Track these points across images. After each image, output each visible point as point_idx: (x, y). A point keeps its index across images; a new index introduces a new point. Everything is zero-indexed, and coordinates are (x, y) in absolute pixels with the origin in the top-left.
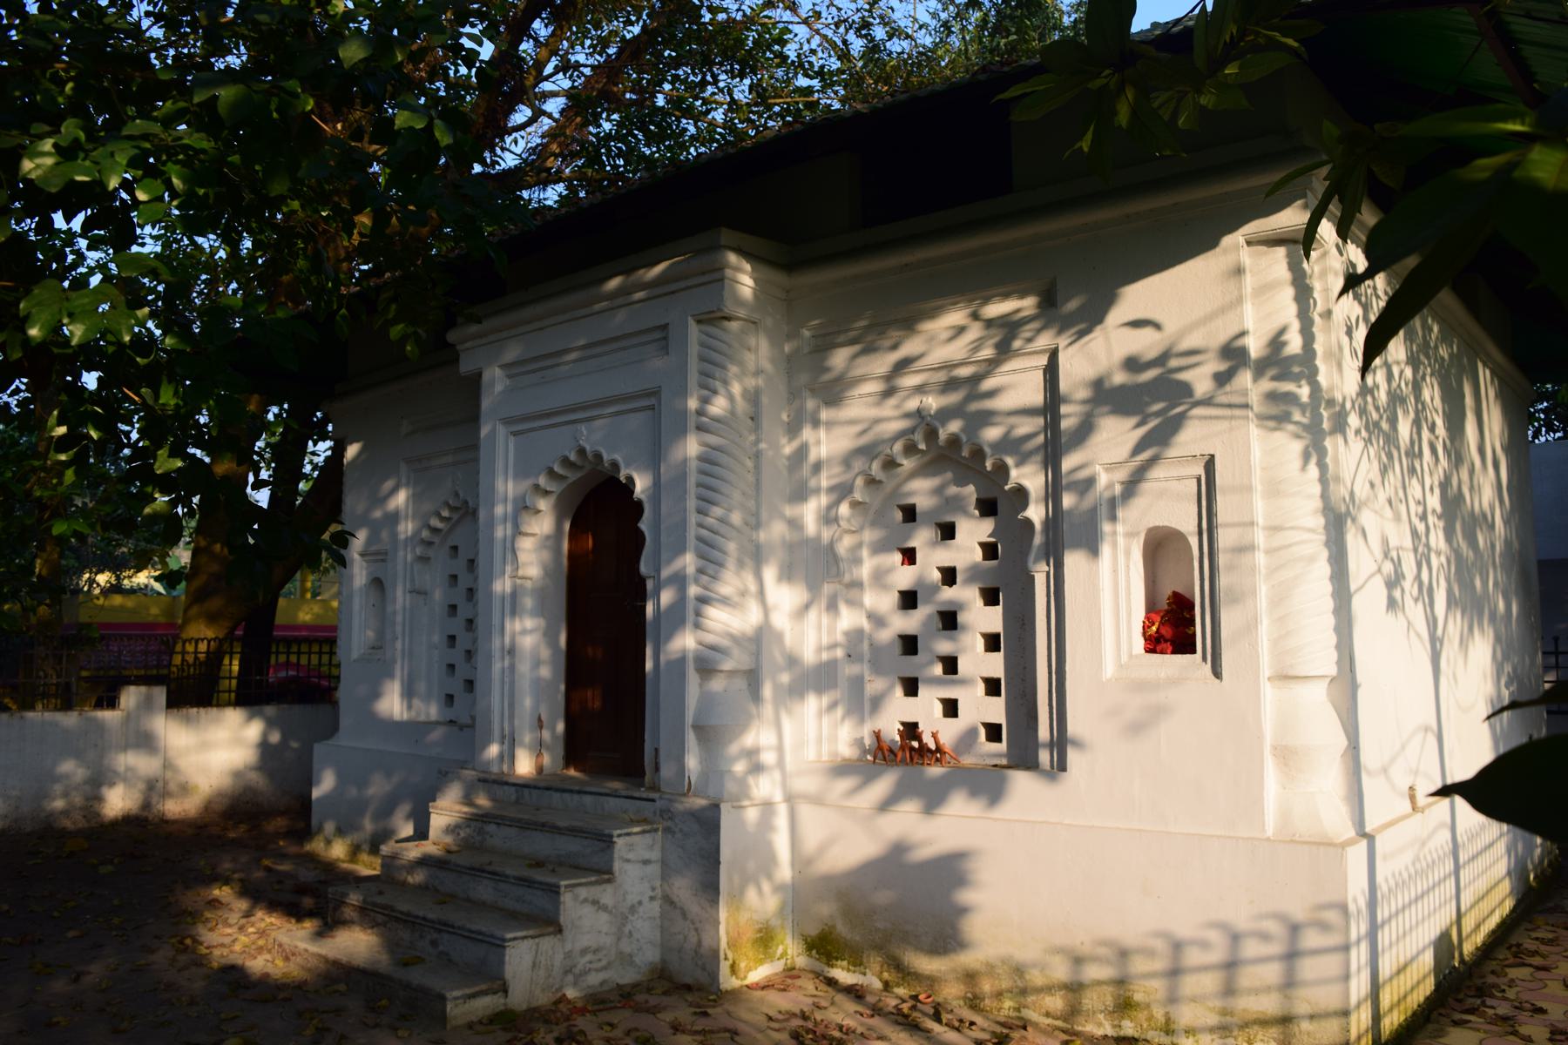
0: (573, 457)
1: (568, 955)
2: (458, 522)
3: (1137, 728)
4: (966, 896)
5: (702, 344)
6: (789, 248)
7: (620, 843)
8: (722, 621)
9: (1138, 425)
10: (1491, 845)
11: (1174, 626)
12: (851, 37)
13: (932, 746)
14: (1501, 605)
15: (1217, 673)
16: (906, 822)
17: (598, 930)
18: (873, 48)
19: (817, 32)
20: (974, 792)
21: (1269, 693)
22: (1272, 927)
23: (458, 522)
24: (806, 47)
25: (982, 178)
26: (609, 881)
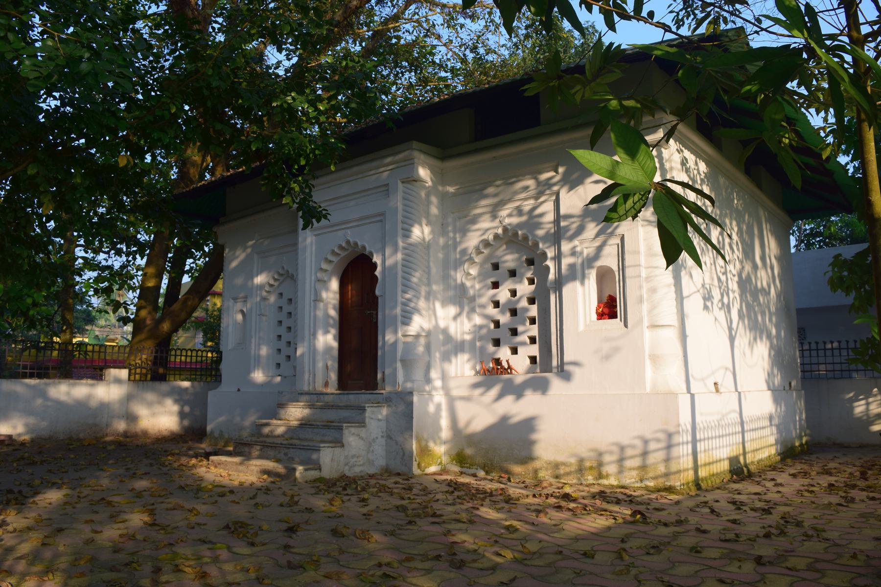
0: (344, 244)
1: (346, 457)
2: (283, 281)
3: (607, 357)
4: (535, 436)
5: (404, 192)
6: (443, 149)
7: (368, 410)
8: (418, 324)
9: (597, 225)
10: (763, 428)
11: (609, 308)
13: (506, 367)
14: (774, 331)
15: (626, 326)
17: (358, 449)
18: (478, 60)
19: (451, 50)
20: (535, 390)
21: (647, 333)
23: (283, 281)
24: (445, 58)
25: (499, 122)
26: (364, 427)
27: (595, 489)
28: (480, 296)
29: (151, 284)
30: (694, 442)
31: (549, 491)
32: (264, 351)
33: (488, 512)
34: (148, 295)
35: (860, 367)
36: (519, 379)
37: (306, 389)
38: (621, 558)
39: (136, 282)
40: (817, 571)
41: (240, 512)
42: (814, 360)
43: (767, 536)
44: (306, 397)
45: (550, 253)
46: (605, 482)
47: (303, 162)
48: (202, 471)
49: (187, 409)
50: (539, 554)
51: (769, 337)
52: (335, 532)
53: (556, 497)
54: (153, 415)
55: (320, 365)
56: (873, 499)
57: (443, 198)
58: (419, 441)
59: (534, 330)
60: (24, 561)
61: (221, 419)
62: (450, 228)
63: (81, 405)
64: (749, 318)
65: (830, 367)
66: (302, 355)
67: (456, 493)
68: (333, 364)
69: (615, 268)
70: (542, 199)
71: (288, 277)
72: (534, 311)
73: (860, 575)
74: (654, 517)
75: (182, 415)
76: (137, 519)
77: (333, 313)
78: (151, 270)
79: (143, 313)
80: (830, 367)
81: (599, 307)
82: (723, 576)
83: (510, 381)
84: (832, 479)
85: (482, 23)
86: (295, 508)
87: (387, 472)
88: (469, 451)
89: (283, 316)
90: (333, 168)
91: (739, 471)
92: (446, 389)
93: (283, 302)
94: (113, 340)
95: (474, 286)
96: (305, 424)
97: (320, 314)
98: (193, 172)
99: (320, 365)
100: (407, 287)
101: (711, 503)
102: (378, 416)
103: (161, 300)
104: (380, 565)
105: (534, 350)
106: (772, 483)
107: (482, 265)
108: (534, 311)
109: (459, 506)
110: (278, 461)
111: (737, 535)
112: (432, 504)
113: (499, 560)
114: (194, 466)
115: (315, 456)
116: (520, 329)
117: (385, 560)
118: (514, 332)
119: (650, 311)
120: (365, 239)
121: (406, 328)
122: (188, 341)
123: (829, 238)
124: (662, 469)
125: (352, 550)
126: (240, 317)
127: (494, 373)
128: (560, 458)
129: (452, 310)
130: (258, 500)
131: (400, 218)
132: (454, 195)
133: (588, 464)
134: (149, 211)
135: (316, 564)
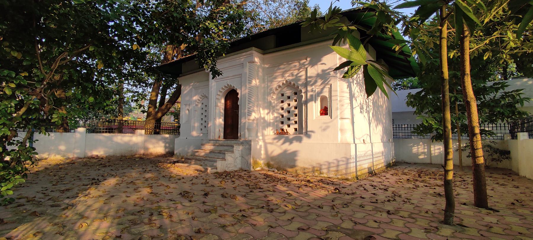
3: (324, 130)
4: (296, 158)
6: (264, 50)
8: (254, 115)
11: (325, 111)
12: (272, 15)
15: (331, 118)
16: (286, 146)
17: (231, 161)
20: (297, 141)
21: (340, 121)
22: (344, 159)
25: (292, 37)
27: (319, 178)
28: (277, 106)
29: (154, 99)
30: (356, 162)
31: (302, 178)
32: (196, 125)
33: (281, 187)
34: (152, 102)
35: (416, 134)
36: (291, 137)
37: (212, 138)
38: (334, 209)
39: (148, 97)
40: (413, 218)
41: (187, 187)
42: (398, 131)
43: (389, 201)
44: (212, 142)
45: (303, 91)
46: (322, 175)
47: (213, 51)
48: (172, 169)
49: (167, 145)
50: (301, 206)
51: (382, 123)
52: (223, 196)
53: (305, 181)
54: (154, 147)
55: (217, 130)
56: (426, 186)
57: (264, 69)
58: (253, 159)
59: (297, 119)
60: (95, 211)
61: (181, 149)
62: (266, 80)
63: (127, 144)
64: (376, 116)
65: (403, 134)
66: (210, 126)
67: (268, 179)
68: (222, 130)
69: (328, 96)
70: (301, 70)
71: (205, 97)
72: (296, 112)
73: (432, 221)
74: (343, 191)
75: (166, 147)
76: (145, 192)
77: (223, 111)
78: (154, 94)
79: (151, 110)
80: (403, 134)
81: (321, 110)
82: (375, 219)
83: (288, 137)
84: (408, 177)
85: (278, 4)
86: (207, 185)
87: (242, 170)
88: (272, 163)
89: (203, 111)
90: (224, 55)
91: (372, 173)
92: (264, 140)
93: (204, 106)
94: (140, 118)
95: (274, 102)
96: (212, 152)
97: (217, 111)
98: (170, 57)
99: (217, 130)
100: (250, 102)
101: (363, 186)
102: (238, 149)
103: (158, 104)
104: (241, 211)
105: (296, 126)
106: (385, 178)
107: (278, 94)
108: (296, 112)
109: (269, 184)
110: (201, 165)
111: (377, 200)
112: (259, 183)
113: (287, 208)
114: (169, 167)
115: (215, 164)
116: (291, 118)
117: (243, 208)
118: (289, 119)
119: (341, 113)
120: (235, 84)
121: (249, 117)
122: (168, 120)
123: (404, 86)
124: (344, 171)
125: (230, 204)
126: (187, 112)
127: (281, 133)
128: (306, 166)
129: (266, 111)
130: (193, 182)
131: (247, 76)
132: (268, 68)
133: (316, 169)
134: (150, 71)
135: (216, 211)
